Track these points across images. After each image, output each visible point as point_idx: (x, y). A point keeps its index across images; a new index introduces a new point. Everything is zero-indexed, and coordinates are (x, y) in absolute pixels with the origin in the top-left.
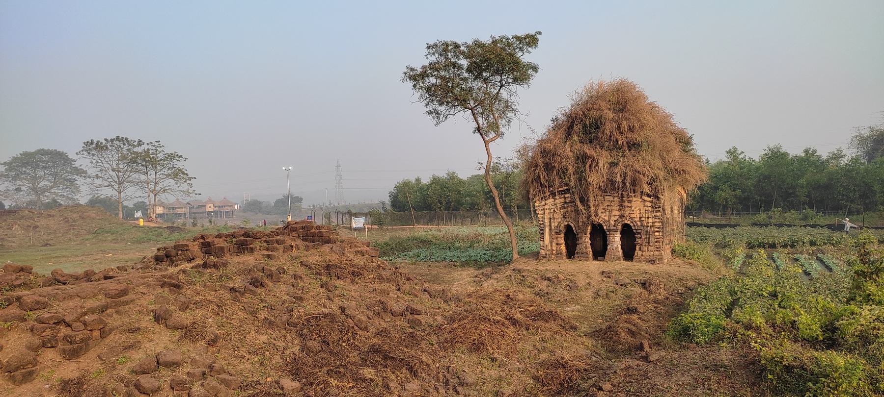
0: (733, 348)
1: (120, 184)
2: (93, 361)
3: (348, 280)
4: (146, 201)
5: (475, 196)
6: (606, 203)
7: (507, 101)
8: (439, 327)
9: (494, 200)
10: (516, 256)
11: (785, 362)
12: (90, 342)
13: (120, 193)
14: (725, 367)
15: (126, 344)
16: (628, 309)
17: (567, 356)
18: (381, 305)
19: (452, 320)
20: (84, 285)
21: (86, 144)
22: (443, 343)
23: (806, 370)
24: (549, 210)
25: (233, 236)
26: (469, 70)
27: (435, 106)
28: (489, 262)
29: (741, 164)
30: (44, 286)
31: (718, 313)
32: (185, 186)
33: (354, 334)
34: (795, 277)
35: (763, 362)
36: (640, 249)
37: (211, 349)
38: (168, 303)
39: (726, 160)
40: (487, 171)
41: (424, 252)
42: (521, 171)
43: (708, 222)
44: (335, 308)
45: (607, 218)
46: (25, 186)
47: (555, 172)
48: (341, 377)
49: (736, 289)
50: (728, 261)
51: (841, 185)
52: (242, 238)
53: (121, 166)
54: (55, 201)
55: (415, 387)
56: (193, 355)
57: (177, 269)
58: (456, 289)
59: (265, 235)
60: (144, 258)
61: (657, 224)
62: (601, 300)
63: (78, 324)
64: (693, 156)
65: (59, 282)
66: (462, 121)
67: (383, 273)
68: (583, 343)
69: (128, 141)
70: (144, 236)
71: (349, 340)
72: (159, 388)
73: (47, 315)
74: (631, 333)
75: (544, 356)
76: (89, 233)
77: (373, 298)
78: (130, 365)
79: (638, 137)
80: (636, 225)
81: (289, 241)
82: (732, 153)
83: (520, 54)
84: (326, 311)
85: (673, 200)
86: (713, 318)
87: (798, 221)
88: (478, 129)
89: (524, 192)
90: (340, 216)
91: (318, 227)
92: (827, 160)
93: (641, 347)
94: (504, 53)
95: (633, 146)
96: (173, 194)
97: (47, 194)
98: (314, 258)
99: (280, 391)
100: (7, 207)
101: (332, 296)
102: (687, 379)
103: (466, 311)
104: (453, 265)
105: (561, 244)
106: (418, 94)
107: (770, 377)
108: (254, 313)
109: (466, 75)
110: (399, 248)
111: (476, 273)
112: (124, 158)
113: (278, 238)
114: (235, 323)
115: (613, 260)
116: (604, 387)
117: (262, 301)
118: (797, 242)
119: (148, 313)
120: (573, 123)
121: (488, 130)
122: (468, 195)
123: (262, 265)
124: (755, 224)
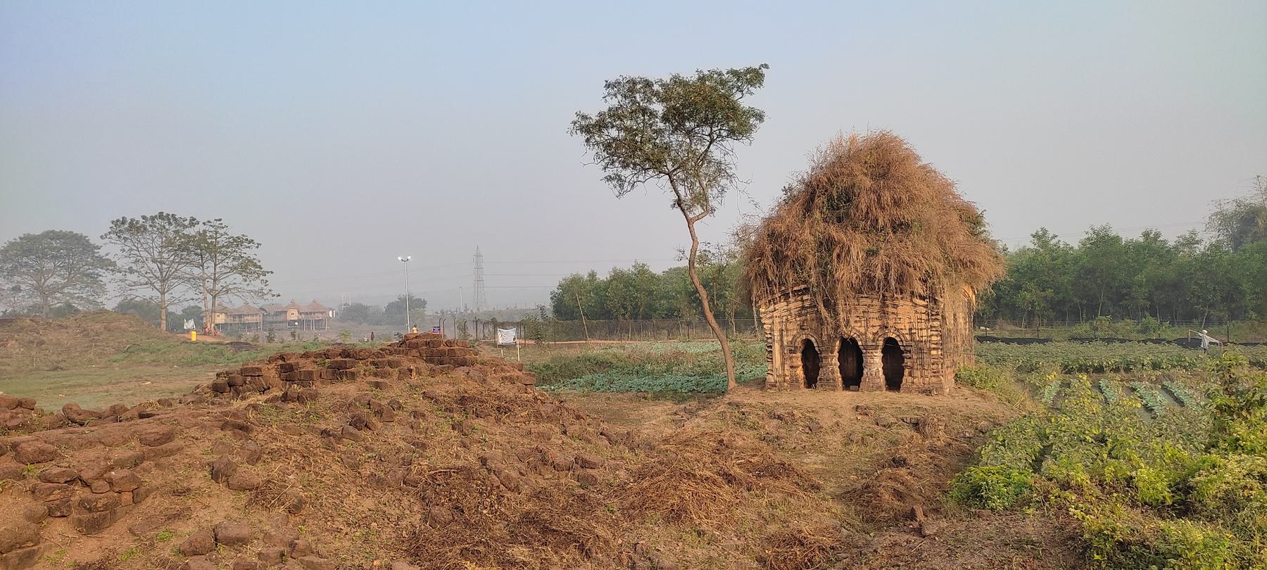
1: (163, 280)
4: (201, 305)
5: (674, 297)
7: (720, 163)
8: (622, 487)
10: (732, 384)
11: (1118, 537)
12: (118, 509)
13: (163, 293)
14: (1033, 543)
16: (894, 460)
17: (806, 528)
19: (641, 476)
21: (116, 223)
22: (627, 509)
23: (1148, 547)
24: (780, 318)
25: (326, 355)
26: (665, 119)
27: (616, 169)
30: (52, 427)
31: (1021, 465)
32: (257, 284)
33: (500, 497)
34: (1130, 414)
35: (1086, 536)
37: (292, 519)
38: (231, 453)
39: (1032, 246)
40: (691, 262)
41: (600, 379)
42: (740, 263)
43: (1006, 335)
44: (472, 459)
45: (862, 330)
46: (27, 283)
47: (788, 265)
49: (1048, 431)
50: (1035, 391)
51: (1196, 283)
52: (339, 359)
53: (165, 255)
54: (69, 306)
56: (267, 528)
57: (245, 403)
58: (646, 431)
60: (198, 387)
61: (934, 338)
62: (854, 448)
63: (101, 483)
64: (985, 241)
65: (74, 421)
66: (654, 191)
67: (542, 409)
68: (829, 510)
69: (175, 220)
71: (492, 506)
73: (56, 470)
74: (899, 495)
75: (772, 528)
76: (118, 351)
77: (526, 444)
78: (175, 542)
79: (906, 214)
80: (903, 339)
81: (406, 363)
82: (1041, 237)
83: (738, 95)
84: (460, 463)
85: (958, 303)
86: (1015, 473)
88: (679, 203)
90: (480, 327)
91: (449, 343)
92: (1176, 248)
93: (912, 515)
95: (900, 226)
96: (240, 296)
98: (443, 387)
106: (592, 152)
107: (1097, 557)
108: (355, 467)
109: (661, 125)
111: (675, 408)
112: (169, 243)
113: (391, 358)
119: (203, 467)
120: (813, 193)
121: (693, 204)
122: (663, 297)
123: (368, 398)
124: (1073, 339)
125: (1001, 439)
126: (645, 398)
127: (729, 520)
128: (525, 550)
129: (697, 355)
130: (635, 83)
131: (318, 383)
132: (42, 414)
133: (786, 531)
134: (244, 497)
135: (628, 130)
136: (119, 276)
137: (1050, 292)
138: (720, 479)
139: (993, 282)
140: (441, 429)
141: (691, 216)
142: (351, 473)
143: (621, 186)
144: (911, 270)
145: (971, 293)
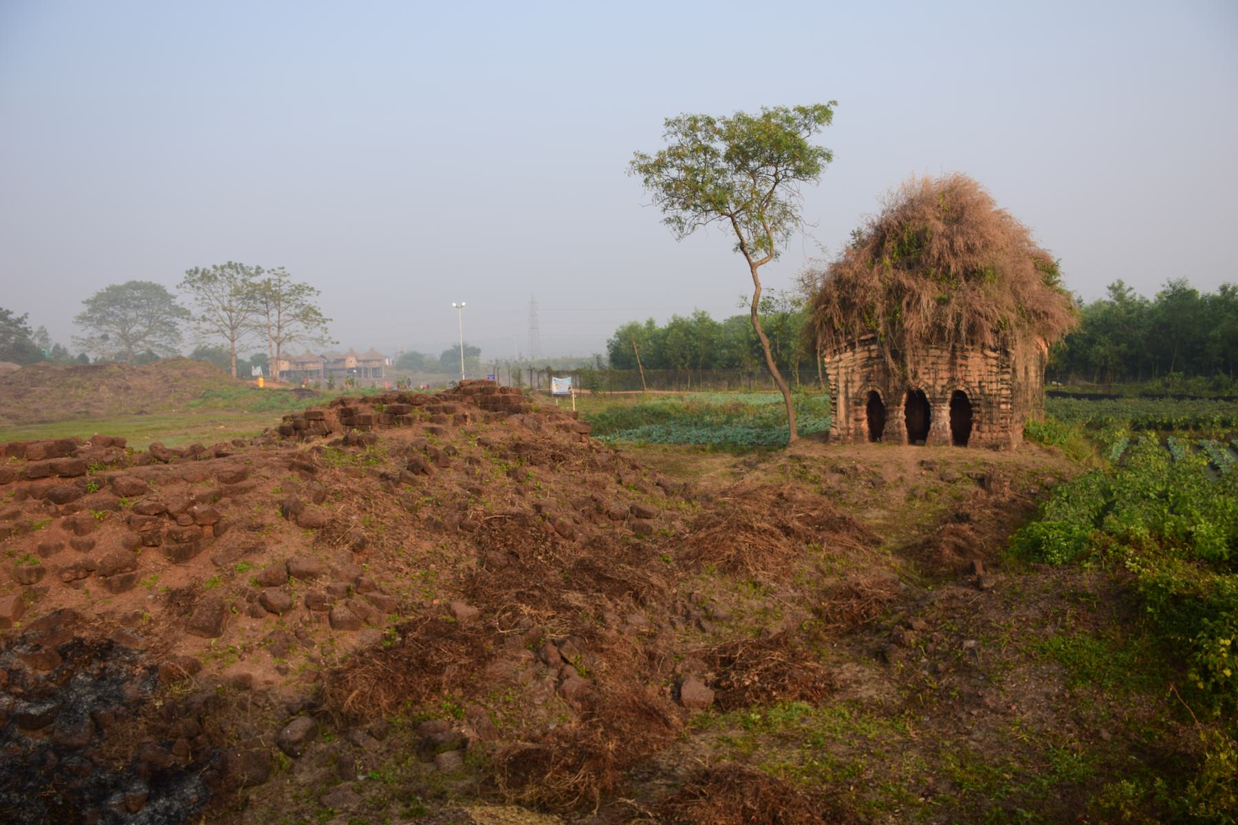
0: (1100, 569)
1: (233, 328)
2: (205, 567)
3: (546, 467)
4: (267, 352)
5: (735, 347)
6: (930, 360)
8: (678, 538)
9: (763, 354)
10: (794, 437)
11: (1173, 590)
12: (201, 541)
13: (233, 341)
14: (1088, 596)
15: (247, 546)
16: (957, 516)
17: (864, 581)
18: (593, 504)
19: (697, 526)
20: (191, 464)
21: (190, 273)
22: (683, 560)
23: (1201, 601)
24: (845, 368)
25: (384, 400)
26: (728, 158)
27: (677, 210)
28: (754, 446)
29: (1130, 307)
30: (141, 464)
32: (317, 332)
33: (554, 544)
34: (1196, 471)
35: (1141, 589)
36: (978, 429)
37: (356, 557)
38: (298, 492)
39: (1108, 299)
40: (754, 310)
41: (657, 430)
42: (805, 311)
43: (1078, 390)
44: (527, 506)
45: (931, 382)
46: (114, 332)
47: (855, 313)
48: (536, 603)
49: (1112, 487)
50: (1103, 448)
52: (396, 404)
53: (234, 304)
54: (150, 353)
55: (641, 620)
56: (334, 564)
57: (308, 447)
58: (704, 483)
59: (427, 399)
60: (266, 430)
61: (1004, 392)
62: (918, 504)
63: (185, 516)
64: (1060, 292)
65: (159, 459)
66: (716, 233)
67: (598, 458)
68: (888, 564)
69: (242, 268)
70: (264, 401)
71: (546, 552)
72: (291, 605)
73: (146, 503)
74: (959, 550)
75: (830, 581)
76: (195, 396)
77: (580, 493)
78: (253, 573)
79: (980, 262)
80: (973, 391)
81: (461, 410)
82: (1117, 289)
83: (805, 133)
84: (515, 510)
85: (1030, 355)
86: (1076, 528)
87: (1205, 392)
88: (742, 246)
89: (809, 341)
90: (535, 376)
91: (503, 390)
93: (971, 569)
94: (780, 133)
95: (973, 274)
96: (303, 344)
97: (141, 343)
98: (497, 433)
99: (452, 619)
100: (91, 361)
101: (522, 489)
102: (1032, 613)
103: (718, 514)
104: (700, 448)
105: (861, 420)
106: (651, 192)
107: (1150, 609)
108: (413, 510)
109: (724, 165)
110: (623, 422)
112: (237, 292)
113: (445, 404)
114: (390, 523)
115: (976, 446)
116: (915, 624)
117: (424, 493)
118: (1204, 422)
119: (273, 504)
120: (884, 237)
121: (759, 247)
122: (724, 346)
123: (424, 443)
124: (1144, 395)
125: (1065, 495)
126: (703, 450)
127: (786, 573)
128: (580, 596)
129: (759, 406)
130: (696, 121)
131: (376, 428)
132: (132, 451)
133: (843, 585)
134: (312, 535)
135: (688, 169)
136: (193, 324)
137: (1123, 347)
138: (777, 531)
139: (1066, 333)
140: (496, 474)
141: (754, 260)
142: (410, 515)
143: (681, 228)
144: (983, 320)
145: (1043, 345)
